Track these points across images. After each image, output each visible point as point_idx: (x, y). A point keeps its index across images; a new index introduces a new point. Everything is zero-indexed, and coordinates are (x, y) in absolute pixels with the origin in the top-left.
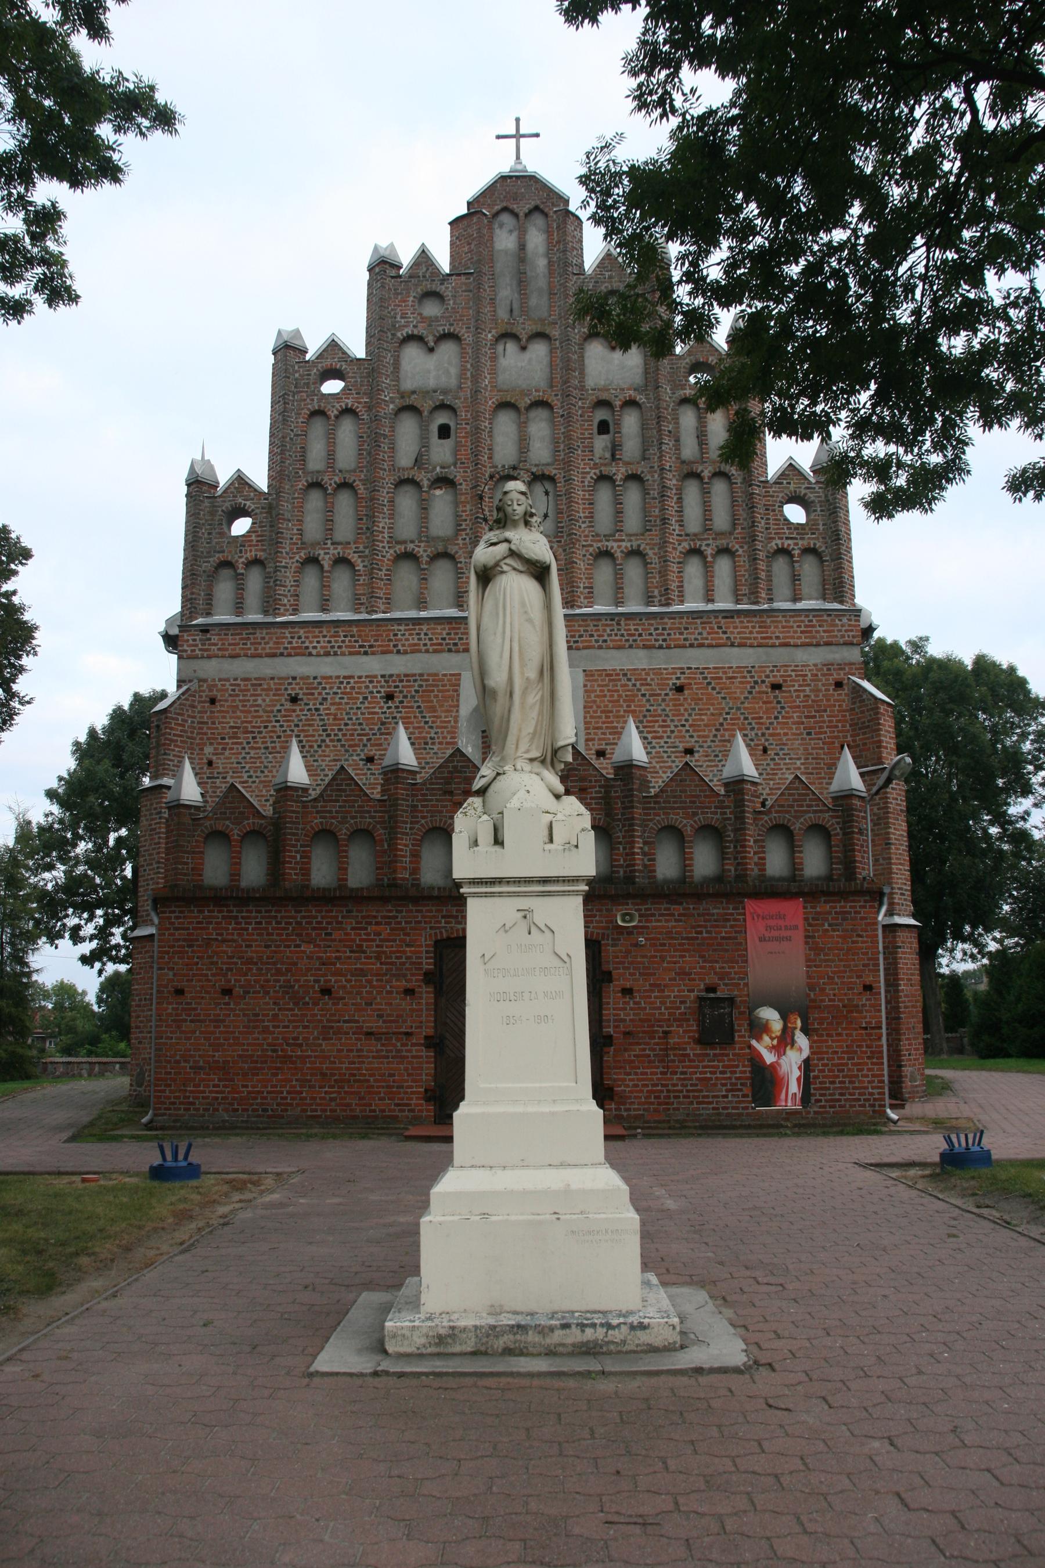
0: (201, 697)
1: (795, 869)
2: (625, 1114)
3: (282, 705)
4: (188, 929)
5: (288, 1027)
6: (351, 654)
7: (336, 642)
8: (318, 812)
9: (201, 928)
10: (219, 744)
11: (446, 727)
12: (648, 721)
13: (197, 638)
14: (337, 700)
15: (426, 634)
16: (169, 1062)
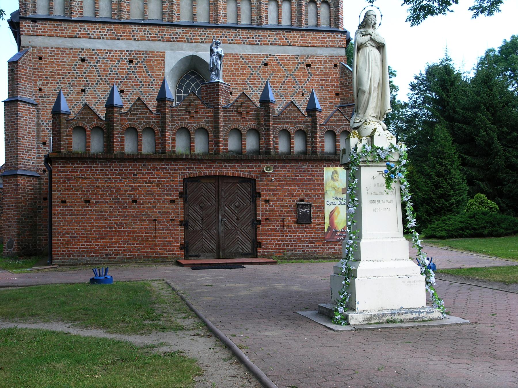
0: (34, 55)
1: (336, 150)
2: (266, 253)
3: (77, 62)
4: (67, 172)
5: (117, 217)
6: (111, 39)
7: (104, 32)
8: (128, 119)
9: (74, 172)
10: (44, 80)
11: (158, 78)
12: (251, 79)
13: (30, 25)
14: (105, 62)
15: (148, 32)
16: (60, 235)
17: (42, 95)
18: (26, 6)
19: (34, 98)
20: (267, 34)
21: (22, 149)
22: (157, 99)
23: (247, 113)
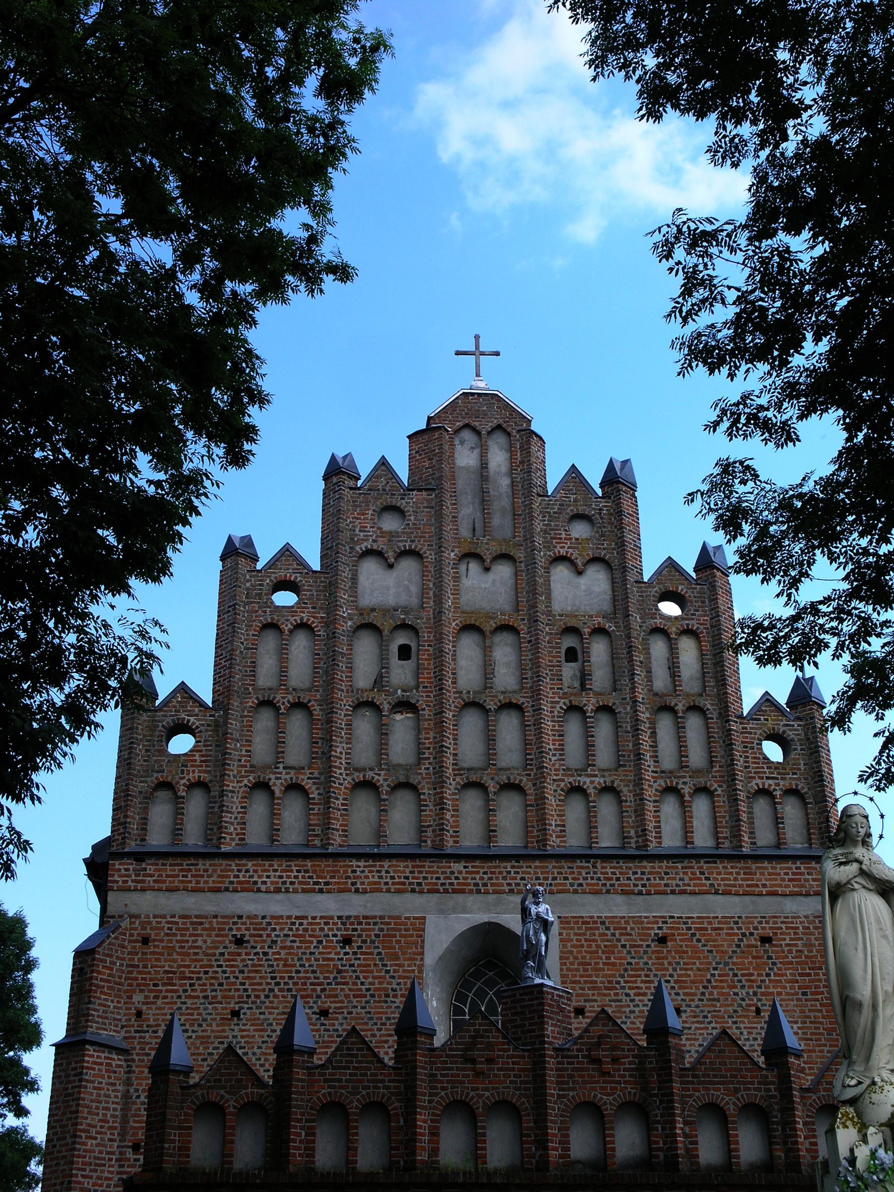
0: (131, 935)
3: (225, 947)
6: (304, 891)
7: (288, 877)
8: (325, 1081)
10: (150, 991)
12: (629, 976)
13: (131, 867)
15: (387, 872)
17: (141, 1026)
18: (125, 828)
19: (123, 1034)
20: (661, 867)
21: (83, 1164)
22: (395, 1030)
23: (615, 1060)
